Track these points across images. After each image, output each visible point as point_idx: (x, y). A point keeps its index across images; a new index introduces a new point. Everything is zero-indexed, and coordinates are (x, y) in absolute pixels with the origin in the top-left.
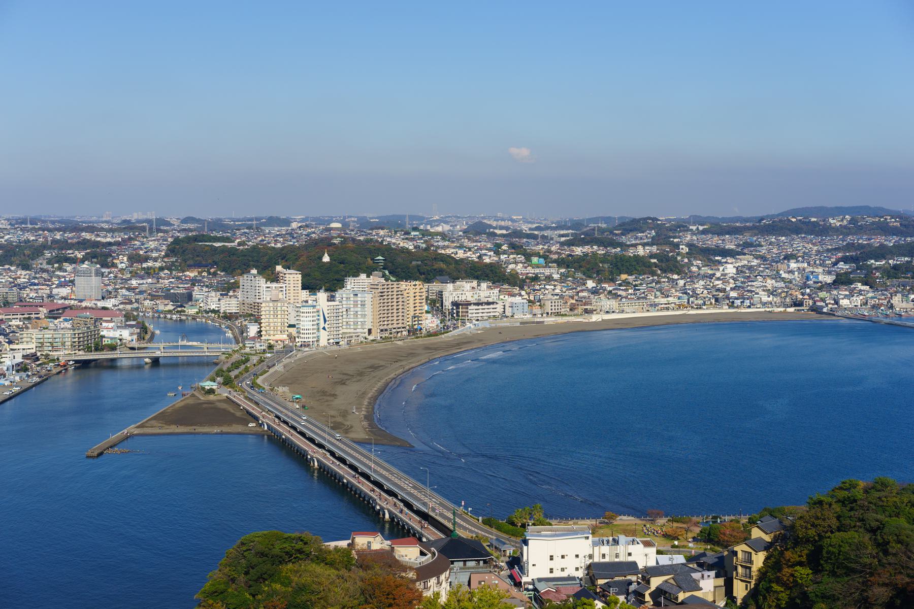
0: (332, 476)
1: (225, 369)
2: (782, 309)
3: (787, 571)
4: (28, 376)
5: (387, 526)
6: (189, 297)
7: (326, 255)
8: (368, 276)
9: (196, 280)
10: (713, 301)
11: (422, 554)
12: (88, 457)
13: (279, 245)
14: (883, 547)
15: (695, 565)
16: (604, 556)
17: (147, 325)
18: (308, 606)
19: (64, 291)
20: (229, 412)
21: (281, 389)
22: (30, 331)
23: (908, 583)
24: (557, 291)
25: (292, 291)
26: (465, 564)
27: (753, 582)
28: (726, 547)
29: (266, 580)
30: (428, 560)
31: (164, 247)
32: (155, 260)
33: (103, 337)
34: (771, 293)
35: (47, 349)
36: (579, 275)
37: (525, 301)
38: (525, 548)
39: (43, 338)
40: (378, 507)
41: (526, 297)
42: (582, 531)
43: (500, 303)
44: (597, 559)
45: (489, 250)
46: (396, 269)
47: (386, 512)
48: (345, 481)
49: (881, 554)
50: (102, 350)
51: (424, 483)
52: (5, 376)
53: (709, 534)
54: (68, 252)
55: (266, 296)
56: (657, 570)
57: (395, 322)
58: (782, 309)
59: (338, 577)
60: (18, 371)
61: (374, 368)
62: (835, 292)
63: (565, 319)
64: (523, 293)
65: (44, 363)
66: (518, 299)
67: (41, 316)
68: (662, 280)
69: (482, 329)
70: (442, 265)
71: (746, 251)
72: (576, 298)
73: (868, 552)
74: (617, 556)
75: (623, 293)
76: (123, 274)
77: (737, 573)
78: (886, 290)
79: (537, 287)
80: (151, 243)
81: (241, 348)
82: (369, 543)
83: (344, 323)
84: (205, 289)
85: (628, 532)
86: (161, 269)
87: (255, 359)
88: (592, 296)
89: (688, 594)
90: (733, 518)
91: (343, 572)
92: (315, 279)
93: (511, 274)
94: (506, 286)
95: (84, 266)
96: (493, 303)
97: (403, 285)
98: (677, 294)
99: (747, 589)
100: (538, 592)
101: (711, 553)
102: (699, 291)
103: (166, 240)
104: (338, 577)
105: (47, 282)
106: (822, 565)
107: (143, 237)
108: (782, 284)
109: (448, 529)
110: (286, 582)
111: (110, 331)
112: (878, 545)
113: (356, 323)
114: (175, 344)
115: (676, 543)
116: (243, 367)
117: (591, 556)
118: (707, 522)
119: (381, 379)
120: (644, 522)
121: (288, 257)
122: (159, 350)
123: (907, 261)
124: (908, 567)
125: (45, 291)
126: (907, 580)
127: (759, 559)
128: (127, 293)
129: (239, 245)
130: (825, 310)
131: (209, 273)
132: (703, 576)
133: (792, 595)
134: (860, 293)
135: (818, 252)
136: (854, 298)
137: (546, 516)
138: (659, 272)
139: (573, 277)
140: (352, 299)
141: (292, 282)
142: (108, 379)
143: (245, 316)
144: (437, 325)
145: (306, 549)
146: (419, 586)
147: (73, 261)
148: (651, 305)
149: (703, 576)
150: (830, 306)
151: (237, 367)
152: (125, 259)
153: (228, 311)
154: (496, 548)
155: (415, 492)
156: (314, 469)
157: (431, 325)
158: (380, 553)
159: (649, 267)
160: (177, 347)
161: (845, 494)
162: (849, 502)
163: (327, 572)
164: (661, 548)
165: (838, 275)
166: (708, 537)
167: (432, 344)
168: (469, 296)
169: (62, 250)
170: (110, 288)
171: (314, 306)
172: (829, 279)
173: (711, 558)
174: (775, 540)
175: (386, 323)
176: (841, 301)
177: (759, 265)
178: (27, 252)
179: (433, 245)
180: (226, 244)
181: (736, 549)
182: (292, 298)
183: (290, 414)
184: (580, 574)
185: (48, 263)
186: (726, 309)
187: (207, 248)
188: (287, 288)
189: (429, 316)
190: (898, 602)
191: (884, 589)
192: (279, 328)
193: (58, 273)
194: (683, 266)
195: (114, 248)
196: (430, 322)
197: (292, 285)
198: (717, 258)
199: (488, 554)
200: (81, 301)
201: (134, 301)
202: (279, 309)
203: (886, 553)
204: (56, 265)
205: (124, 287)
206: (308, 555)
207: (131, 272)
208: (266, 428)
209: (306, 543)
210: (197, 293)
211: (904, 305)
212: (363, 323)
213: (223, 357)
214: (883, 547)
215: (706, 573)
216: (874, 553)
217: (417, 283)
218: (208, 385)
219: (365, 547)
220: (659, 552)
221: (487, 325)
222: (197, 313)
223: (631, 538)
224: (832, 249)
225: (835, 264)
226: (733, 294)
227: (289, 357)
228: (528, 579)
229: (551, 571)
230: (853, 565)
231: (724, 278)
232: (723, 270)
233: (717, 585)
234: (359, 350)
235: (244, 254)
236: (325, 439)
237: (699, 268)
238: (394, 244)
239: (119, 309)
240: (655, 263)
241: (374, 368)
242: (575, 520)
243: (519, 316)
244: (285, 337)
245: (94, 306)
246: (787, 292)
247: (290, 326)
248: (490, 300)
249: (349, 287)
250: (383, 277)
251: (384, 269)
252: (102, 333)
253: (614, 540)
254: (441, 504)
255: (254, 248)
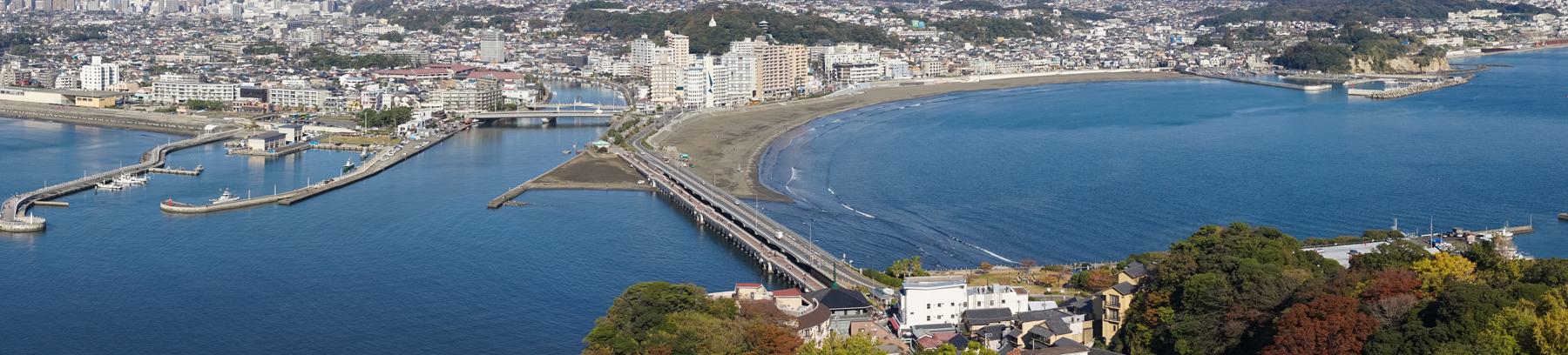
0: (717, 230)
1: (616, 129)
2: (1148, 70)
3: (1150, 311)
4: (436, 132)
5: (770, 277)
6: (585, 61)
7: (713, 19)
8: (753, 40)
9: (591, 44)
10: (1084, 62)
11: (804, 304)
12: (489, 208)
13: (668, 11)
14: (1237, 285)
15: (1066, 310)
16: (979, 303)
17: (545, 86)
18: (692, 352)
19: (470, 54)
20: (620, 169)
21: (669, 149)
22: (439, 90)
23: (1259, 316)
24: (937, 53)
25: (680, 55)
26: (846, 314)
27: (1121, 323)
28: (1094, 292)
29: (651, 327)
30: (810, 309)
31: (562, 13)
32: (554, 25)
33: (505, 97)
34: (1138, 54)
35: (453, 107)
36: (958, 38)
37: (905, 63)
38: (903, 297)
39: (451, 97)
40: (762, 260)
41: (907, 58)
42: (958, 281)
43: (881, 65)
44: (971, 307)
45: (871, 13)
46: (780, 32)
47: (769, 264)
48: (730, 235)
49: (1236, 292)
50: (504, 109)
51: (805, 235)
52: (416, 132)
53: (1079, 281)
54: (474, 17)
55: (656, 60)
56: (1030, 316)
57: (778, 84)
58: (1148, 70)
59: (722, 325)
60: (427, 127)
61: (759, 128)
62: (1196, 53)
63: (944, 80)
64: (903, 55)
65: (451, 121)
66: (897, 61)
67: (449, 77)
68: (1037, 42)
69: (864, 90)
70: (824, 29)
71: (1115, 14)
72: (954, 59)
73: (1225, 290)
74: (992, 303)
75: (1000, 55)
76: (524, 39)
77: (1106, 316)
78: (1242, 51)
79: (918, 50)
80: (550, 9)
81: (632, 110)
82: (752, 293)
83: (730, 86)
84: (599, 53)
85: (1001, 281)
86: (559, 34)
87: (645, 120)
88: (970, 58)
89: (1059, 337)
90: (1103, 265)
91: (728, 321)
92: (702, 43)
93: (891, 36)
94: (886, 49)
95: (489, 30)
96: (874, 65)
97: (786, 48)
98: (1051, 55)
99: (1114, 330)
100: (916, 338)
101: (1081, 298)
102: (1071, 53)
103: (564, 6)
104: (722, 325)
105: (455, 46)
106: (1182, 304)
107: (543, 4)
108: (1148, 46)
109: (830, 280)
110: (672, 330)
111: (511, 93)
112: (1234, 283)
113: (741, 86)
114: (571, 105)
115: (1049, 290)
116: (632, 128)
117: (965, 304)
118: (1077, 270)
119: (765, 138)
120: (1018, 271)
121: (676, 22)
122: (557, 110)
123: (1261, 24)
124: (1259, 302)
125: (453, 54)
126: (1259, 313)
127: (1126, 302)
128: (528, 56)
129: (631, 10)
130: (1187, 70)
131: (603, 38)
132: (1073, 320)
133: (1157, 333)
134: (1219, 53)
135: (1181, 15)
136: (1214, 58)
137: (924, 268)
138: (1034, 35)
139: (952, 40)
140: (737, 62)
141: (680, 46)
142: (509, 137)
143: (636, 79)
144: (819, 87)
145: (691, 299)
146: (802, 334)
147: (479, 26)
148: (1026, 67)
149: (1073, 320)
150: (1192, 66)
151: (628, 128)
152: (527, 24)
153: (620, 74)
154: (875, 297)
155: (798, 246)
156: (700, 225)
157: (813, 87)
158: (762, 303)
159: (1025, 30)
160: (572, 108)
161: (1203, 238)
162: (1208, 247)
163: (710, 321)
164: (1032, 295)
165: (1199, 37)
166: (1078, 283)
167: (816, 105)
168: (851, 59)
169: (469, 15)
170: (512, 52)
171: (701, 70)
172: (1191, 41)
173: (1080, 303)
174: (1140, 284)
175: (769, 85)
176: (1202, 61)
177: (1127, 28)
178: (438, 17)
179: (815, 10)
180: (619, 10)
181: (1104, 294)
182: (680, 62)
183: (677, 172)
184: (956, 321)
185: (456, 28)
186: (1096, 70)
187: (601, 14)
188: (676, 52)
189: (812, 77)
190: (1251, 334)
191: (1240, 323)
192: (668, 91)
193: (465, 37)
194: (1056, 29)
195: (517, 13)
196: (813, 84)
197: (680, 50)
198: (1088, 22)
199: (868, 304)
200: (486, 63)
201: (534, 64)
202: (667, 72)
203: (1240, 290)
204: (463, 30)
205: (525, 51)
206: (692, 305)
207: (531, 37)
208: (654, 185)
209: (690, 294)
210: (591, 56)
211: (1258, 64)
212: (748, 85)
213: (615, 118)
214: (1237, 285)
215: (1076, 317)
216: (1230, 291)
217: (800, 46)
218: (601, 144)
219: (749, 297)
220: (1031, 299)
221: (868, 86)
222: (592, 76)
223: (1005, 287)
224: (1194, 13)
225: (1197, 27)
226: (1103, 56)
227: (677, 118)
228: (907, 327)
229: (929, 318)
230: (1211, 304)
231: (1094, 41)
232: (1094, 33)
233: (1085, 327)
234: (744, 111)
235: (636, 19)
236: (710, 196)
237: (1072, 31)
238: (778, 8)
239: (520, 72)
240: (1030, 26)
241: (759, 128)
242: (951, 271)
243: (899, 77)
244: (673, 99)
245: (498, 69)
246: (1153, 53)
247: (679, 88)
248: (871, 62)
249: (734, 51)
250: (767, 40)
251: (768, 33)
252: (504, 94)
253: (989, 288)
254: (823, 257)
255: (645, 13)
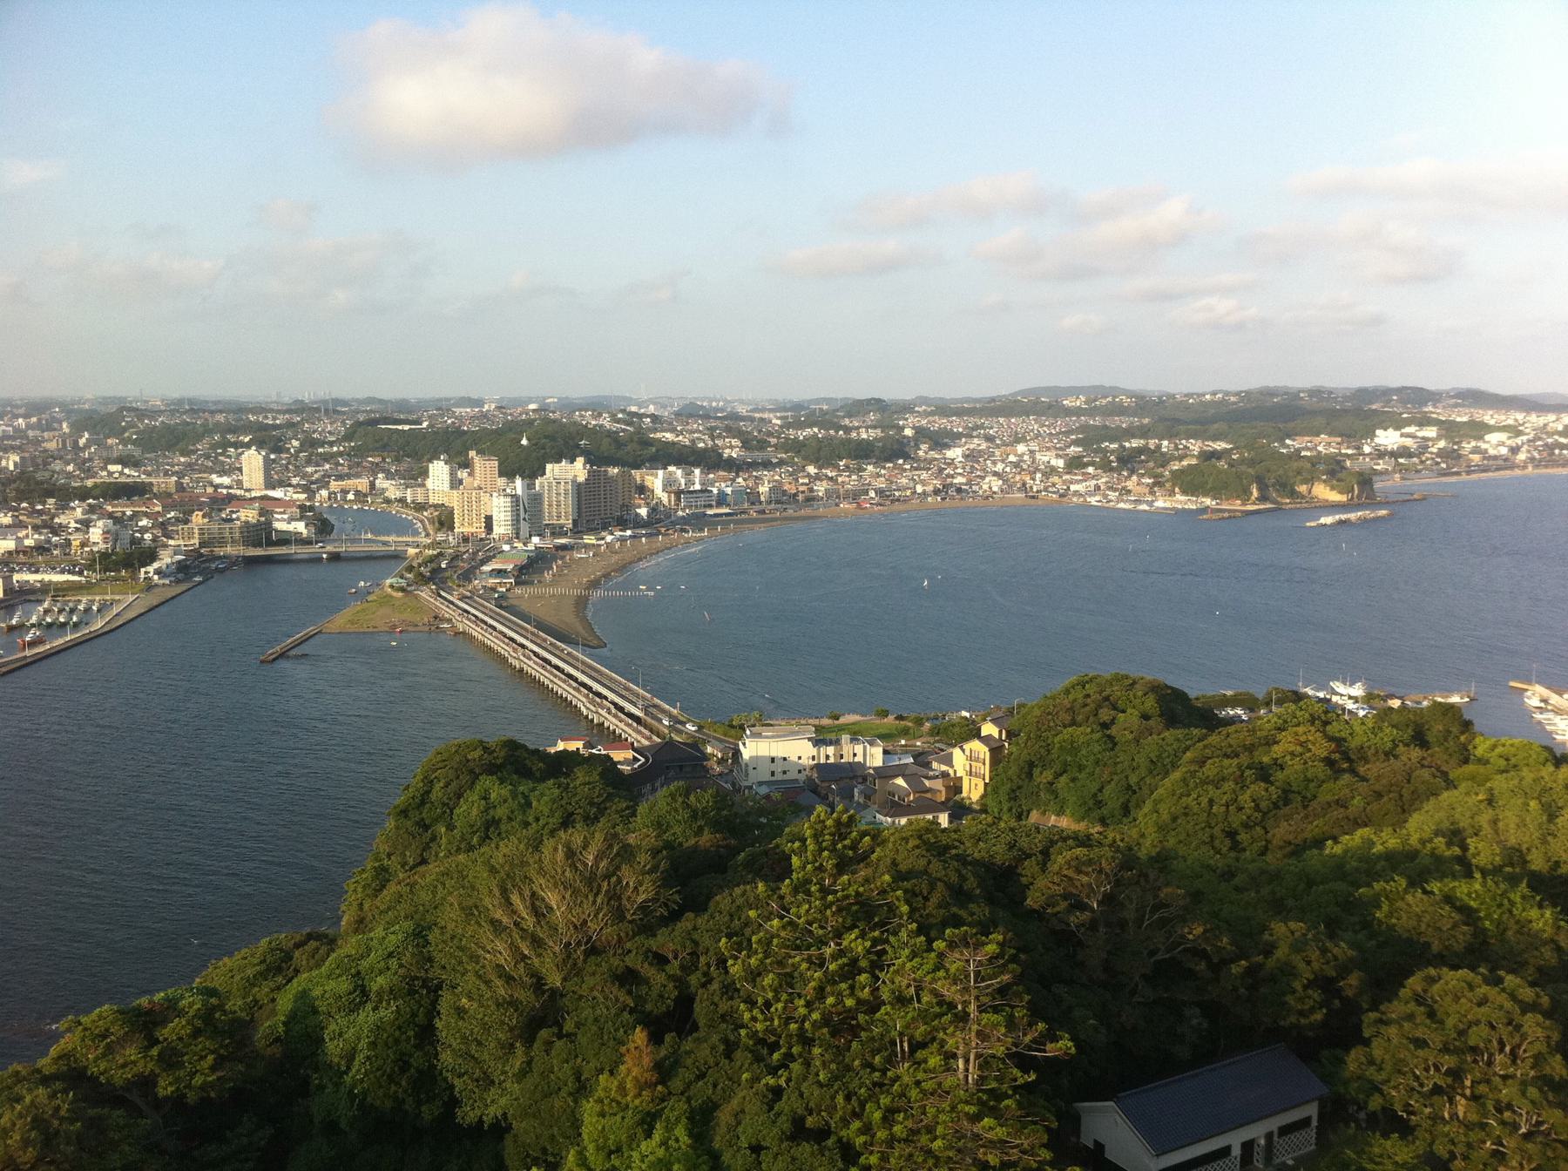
57: (608, 512)
147: (236, 445)
237: (926, 453)
